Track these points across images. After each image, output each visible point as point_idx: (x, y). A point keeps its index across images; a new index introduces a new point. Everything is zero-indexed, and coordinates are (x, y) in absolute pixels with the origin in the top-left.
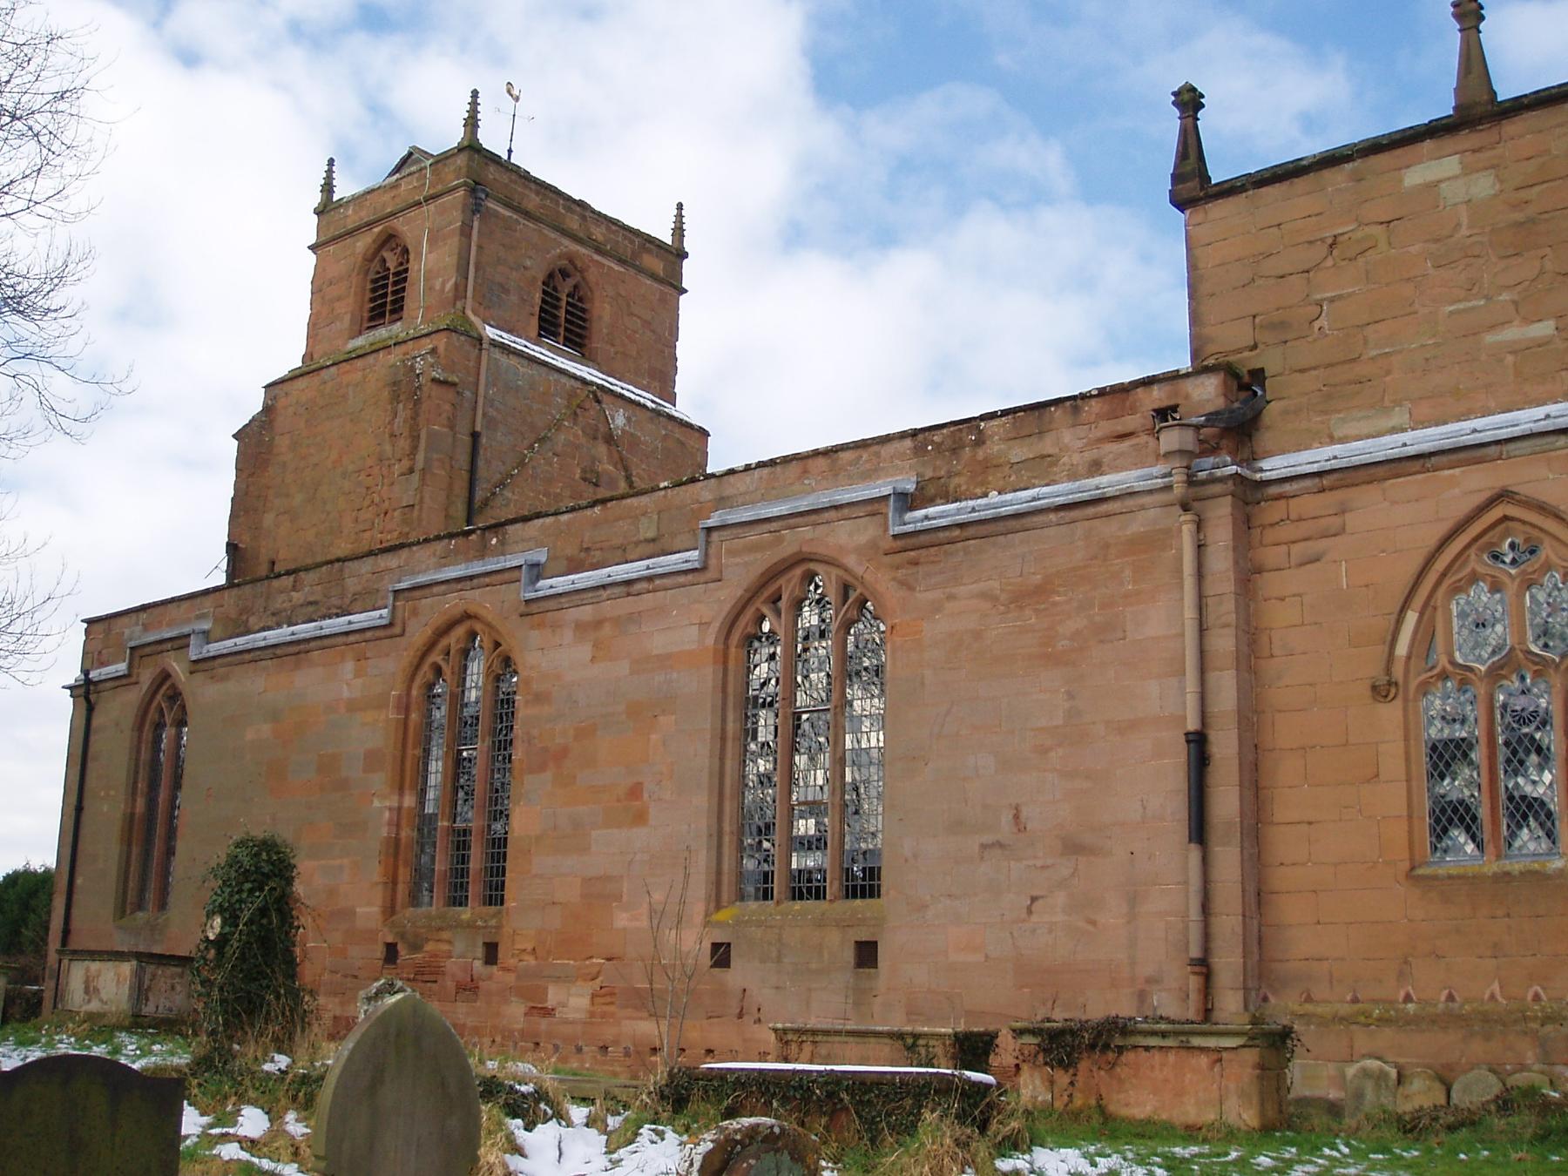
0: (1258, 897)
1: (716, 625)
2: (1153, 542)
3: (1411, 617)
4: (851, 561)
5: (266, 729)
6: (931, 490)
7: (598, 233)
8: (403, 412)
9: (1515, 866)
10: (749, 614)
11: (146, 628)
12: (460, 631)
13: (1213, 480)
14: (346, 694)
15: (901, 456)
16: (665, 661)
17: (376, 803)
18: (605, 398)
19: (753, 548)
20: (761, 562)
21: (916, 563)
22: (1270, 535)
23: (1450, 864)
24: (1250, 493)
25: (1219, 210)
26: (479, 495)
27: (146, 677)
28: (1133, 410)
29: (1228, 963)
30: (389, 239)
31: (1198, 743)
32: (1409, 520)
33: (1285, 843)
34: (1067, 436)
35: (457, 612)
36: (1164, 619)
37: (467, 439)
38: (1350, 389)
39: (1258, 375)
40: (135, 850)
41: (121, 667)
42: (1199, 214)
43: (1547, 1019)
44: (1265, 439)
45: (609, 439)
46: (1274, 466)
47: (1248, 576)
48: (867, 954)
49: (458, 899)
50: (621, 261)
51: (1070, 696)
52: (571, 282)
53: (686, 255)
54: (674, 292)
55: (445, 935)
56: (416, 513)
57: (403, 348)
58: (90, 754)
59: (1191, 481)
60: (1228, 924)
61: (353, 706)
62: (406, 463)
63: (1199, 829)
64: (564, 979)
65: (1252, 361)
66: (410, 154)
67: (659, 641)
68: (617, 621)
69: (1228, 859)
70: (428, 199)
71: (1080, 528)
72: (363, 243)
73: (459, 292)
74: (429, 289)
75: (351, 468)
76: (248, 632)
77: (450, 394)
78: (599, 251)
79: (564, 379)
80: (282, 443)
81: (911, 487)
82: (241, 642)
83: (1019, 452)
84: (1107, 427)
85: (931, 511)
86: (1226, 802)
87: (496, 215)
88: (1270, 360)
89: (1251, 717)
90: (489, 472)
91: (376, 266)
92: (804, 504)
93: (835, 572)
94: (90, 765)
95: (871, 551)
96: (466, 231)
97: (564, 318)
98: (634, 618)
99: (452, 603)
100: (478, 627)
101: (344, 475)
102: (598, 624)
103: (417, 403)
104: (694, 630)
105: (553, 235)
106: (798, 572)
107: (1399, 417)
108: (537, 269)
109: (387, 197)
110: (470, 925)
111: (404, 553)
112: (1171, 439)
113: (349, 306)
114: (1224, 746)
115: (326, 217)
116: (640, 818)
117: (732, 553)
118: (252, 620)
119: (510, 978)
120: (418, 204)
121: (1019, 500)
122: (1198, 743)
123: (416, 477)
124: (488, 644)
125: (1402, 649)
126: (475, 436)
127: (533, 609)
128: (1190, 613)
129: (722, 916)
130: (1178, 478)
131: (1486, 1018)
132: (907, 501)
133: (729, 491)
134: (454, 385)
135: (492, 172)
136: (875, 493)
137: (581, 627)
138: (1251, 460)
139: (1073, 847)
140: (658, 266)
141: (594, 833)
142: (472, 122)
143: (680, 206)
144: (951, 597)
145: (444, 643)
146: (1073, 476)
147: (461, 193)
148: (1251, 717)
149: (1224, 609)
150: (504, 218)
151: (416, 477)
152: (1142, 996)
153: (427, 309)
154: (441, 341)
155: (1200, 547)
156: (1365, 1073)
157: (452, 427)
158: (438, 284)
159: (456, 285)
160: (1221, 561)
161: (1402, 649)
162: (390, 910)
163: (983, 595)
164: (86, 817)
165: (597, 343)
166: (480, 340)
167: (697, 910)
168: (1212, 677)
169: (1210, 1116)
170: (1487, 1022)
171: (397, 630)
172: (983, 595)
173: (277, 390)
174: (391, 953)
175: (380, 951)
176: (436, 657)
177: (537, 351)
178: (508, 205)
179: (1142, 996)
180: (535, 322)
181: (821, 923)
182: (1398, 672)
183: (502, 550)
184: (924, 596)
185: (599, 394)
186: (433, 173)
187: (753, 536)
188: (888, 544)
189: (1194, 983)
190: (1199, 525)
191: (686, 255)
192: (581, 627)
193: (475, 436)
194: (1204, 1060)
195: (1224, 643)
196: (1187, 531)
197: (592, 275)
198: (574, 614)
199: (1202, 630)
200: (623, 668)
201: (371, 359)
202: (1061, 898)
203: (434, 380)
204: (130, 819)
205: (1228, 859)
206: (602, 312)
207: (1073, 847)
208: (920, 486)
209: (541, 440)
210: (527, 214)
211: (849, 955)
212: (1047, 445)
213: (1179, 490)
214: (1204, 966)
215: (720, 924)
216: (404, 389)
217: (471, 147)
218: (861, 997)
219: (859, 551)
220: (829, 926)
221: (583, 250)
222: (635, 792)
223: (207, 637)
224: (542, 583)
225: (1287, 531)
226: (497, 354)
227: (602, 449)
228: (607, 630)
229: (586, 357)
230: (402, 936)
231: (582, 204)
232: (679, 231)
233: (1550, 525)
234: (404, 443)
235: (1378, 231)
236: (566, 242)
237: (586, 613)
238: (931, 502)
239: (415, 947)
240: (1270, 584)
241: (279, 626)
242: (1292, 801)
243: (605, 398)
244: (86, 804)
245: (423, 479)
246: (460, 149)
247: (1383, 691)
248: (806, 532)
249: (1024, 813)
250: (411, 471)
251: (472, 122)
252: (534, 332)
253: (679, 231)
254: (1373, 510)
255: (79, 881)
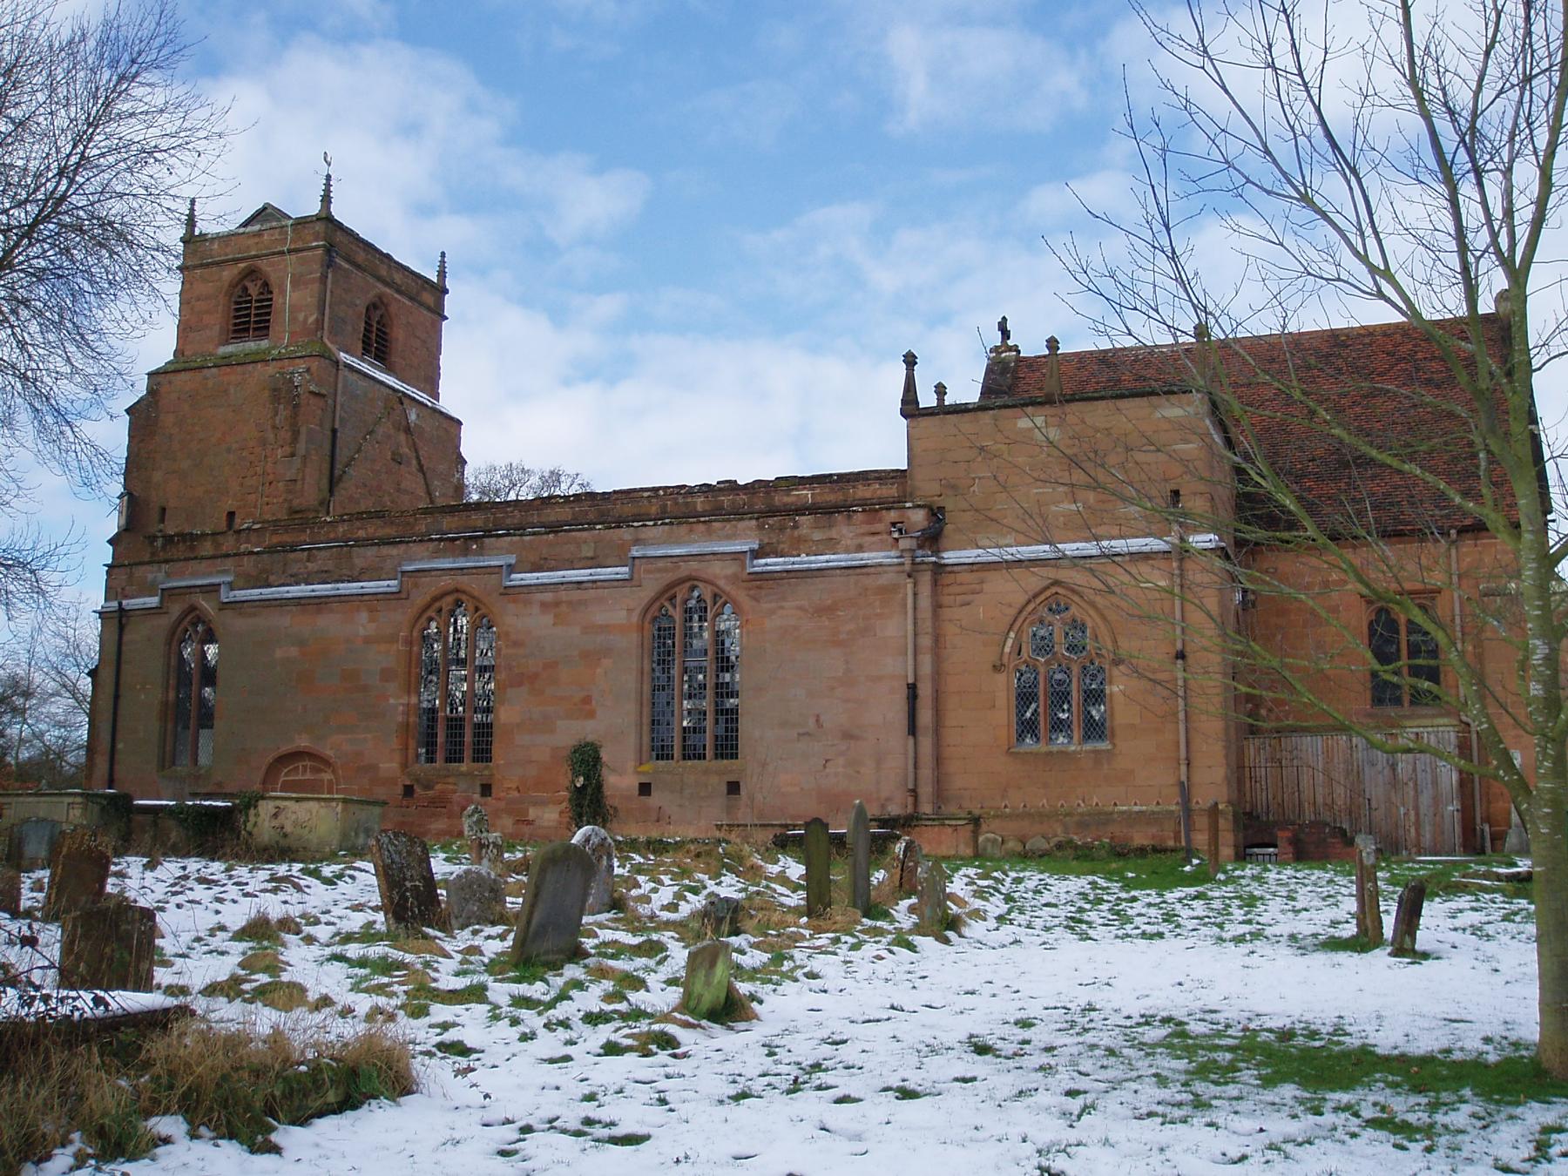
0: (938, 760)
1: (638, 611)
2: (887, 591)
3: (1012, 635)
4: (721, 583)
5: (294, 652)
6: (768, 549)
7: (398, 277)
8: (284, 412)
9: (1055, 749)
10: (657, 604)
11: (168, 575)
12: (450, 599)
13: (923, 563)
14: (362, 632)
15: (751, 529)
16: (605, 628)
17: (392, 701)
18: (406, 401)
19: (660, 570)
20: (670, 577)
21: (759, 588)
22: (946, 590)
23: (1022, 749)
24: (939, 569)
25: (924, 422)
26: (337, 472)
27: (176, 609)
28: (880, 521)
29: (926, 790)
30: (251, 273)
31: (912, 689)
32: (1011, 591)
33: (951, 736)
34: (845, 530)
35: (451, 587)
36: (895, 627)
37: (329, 433)
38: (987, 522)
39: (941, 509)
40: (170, 726)
41: (153, 601)
42: (914, 423)
43: (1067, 815)
44: (944, 542)
45: (408, 430)
46: (950, 557)
47: (937, 607)
48: (733, 788)
49: (454, 756)
50: (411, 299)
51: (847, 662)
52: (379, 313)
53: (446, 291)
54: (436, 317)
55: (451, 780)
56: (299, 486)
57: (280, 364)
58: (124, 657)
59: (913, 564)
60: (926, 772)
61: (368, 640)
62: (288, 449)
63: (913, 729)
64: (542, 803)
65: (939, 501)
66: (264, 209)
67: (600, 617)
68: (570, 603)
69: (926, 743)
70: (290, 251)
71: (853, 579)
72: (229, 274)
73: (319, 323)
74: (293, 319)
75: (235, 446)
76: (270, 586)
77: (321, 402)
78: (399, 291)
79: (383, 388)
80: (168, 420)
81: (756, 547)
82: (267, 592)
83: (817, 535)
84: (866, 528)
85: (769, 560)
86: (925, 716)
87: (340, 267)
88: (949, 504)
89: (938, 675)
90: (342, 455)
91: (238, 291)
92: (694, 549)
93: (710, 588)
94: (124, 667)
95: (734, 579)
96: (324, 278)
97: (377, 345)
98: (583, 603)
99: (446, 582)
100: (464, 597)
101: (229, 451)
102: (557, 604)
103: (296, 406)
104: (624, 613)
105: (371, 280)
106: (688, 585)
107: (1009, 539)
108: (361, 304)
109: (251, 242)
110: (469, 774)
111: (403, 547)
112: (905, 543)
113: (216, 321)
114: (925, 691)
115: (191, 246)
116: (591, 715)
117: (649, 572)
118: (272, 578)
119: (502, 805)
120: (282, 253)
121: (820, 561)
122: (912, 689)
123: (297, 461)
124: (471, 609)
125: (1007, 650)
126: (334, 431)
127: (508, 592)
128: (910, 627)
129: (645, 768)
130: (907, 561)
131: (1041, 815)
132: (756, 554)
133: (643, 536)
134: (323, 396)
135: (339, 237)
136: (738, 548)
137: (544, 606)
138: (936, 552)
139: (848, 736)
140: (428, 298)
141: (559, 723)
142: (326, 199)
143: (443, 255)
144: (782, 608)
145: (437, 605)
146: (847, 551)
147: (320, 251)
148: (938, 675)
149: (927, 625)
150: (345, 270)
151: (297, 461)
152: (883, 806)
153: (292, 334)
154: (315, 364)
155: (915, 594)
156: (988, 840)
157: (321, 425)
158: (301, 317)
159: (317, 320)
160: (925, 602)
161: (1007, 650)
162: (405, 765)
163: (800, 608)
164: (123, 702)
165: (394, 358)
166: (337, 362)
167: (631, 765)
168: (920, 657)
169: (953, 852)
170: (1042, 816)
171: (403, 595)
172: (800, 608)
173: (160, 378)
174: (409, 791)
175: (400, 790)
176: (431, 613)
177: (365, 367)
178: (348, 261)
179: (883, 806)
180: (360, 345)
181: (706, 772)
182: (1005, 660)
183: (481, 552)
184: (765, 606)
185: (403, 398)
186: (293, 231)
187: (661, 564)
188: (745, 576)
189: (910, 800)
190: (915, 584)
191: (446, 291)
192: (544, 606)
193: (334, 431)
194: (950, 830)
195: (926, 641)
196: (910, 587)
197: (393, 309)
198: (539, 596)
199: (915, 635)
200: (576, 631)
201: (250, 367)
202: (841, 761)
203: (312, 393)
204: (165, 704)
205: (926, 743)
206: (398, 334)
207: (848, 736)
208: (761, 547)
209: (370, 433)
210: (358, 266)
211: (724, 788)
212: (833, 533)
213: (907, 568)
214: (914, 792)
215: (643, 773)
216: (283, 393)
217: (326, 218)
218: (729, 810)
219: (726, 577)
220: (713, 771)
221: (388, 290)
222: (587, 700)
223: (231, 586)
224: (514, 576)
225: (952, 589)
226: (346, 372)
227: (402, 437)
228: (564, 608)
229: (389, 370)
230: (418, 781)
231: (388, 256)
232: (442, 274)
233: (1076, 598)
234: (285, 435)
235: (1004, 447)
236: (380, 285)
237: (548, 597)
238: (767, 555)
239: (428, 786)
240: (946, 613)
241: (297, 584)
242: (953, 718)
243: (406, 401)
244: (122, 691)
245: (304, 463)
246: (318, 218)
247: (998, 668)
248: (694, 565)
249: (822, 718)
250: (293, 455)
251: (326, 199)
252: (360, 350)
253: (442, 274)
254: (998, 584)
255: (120, 746)
